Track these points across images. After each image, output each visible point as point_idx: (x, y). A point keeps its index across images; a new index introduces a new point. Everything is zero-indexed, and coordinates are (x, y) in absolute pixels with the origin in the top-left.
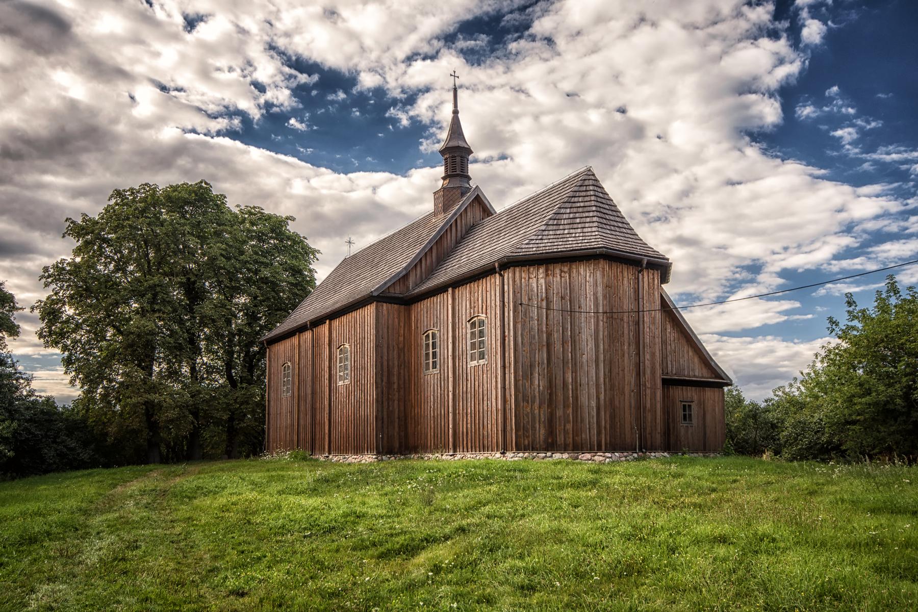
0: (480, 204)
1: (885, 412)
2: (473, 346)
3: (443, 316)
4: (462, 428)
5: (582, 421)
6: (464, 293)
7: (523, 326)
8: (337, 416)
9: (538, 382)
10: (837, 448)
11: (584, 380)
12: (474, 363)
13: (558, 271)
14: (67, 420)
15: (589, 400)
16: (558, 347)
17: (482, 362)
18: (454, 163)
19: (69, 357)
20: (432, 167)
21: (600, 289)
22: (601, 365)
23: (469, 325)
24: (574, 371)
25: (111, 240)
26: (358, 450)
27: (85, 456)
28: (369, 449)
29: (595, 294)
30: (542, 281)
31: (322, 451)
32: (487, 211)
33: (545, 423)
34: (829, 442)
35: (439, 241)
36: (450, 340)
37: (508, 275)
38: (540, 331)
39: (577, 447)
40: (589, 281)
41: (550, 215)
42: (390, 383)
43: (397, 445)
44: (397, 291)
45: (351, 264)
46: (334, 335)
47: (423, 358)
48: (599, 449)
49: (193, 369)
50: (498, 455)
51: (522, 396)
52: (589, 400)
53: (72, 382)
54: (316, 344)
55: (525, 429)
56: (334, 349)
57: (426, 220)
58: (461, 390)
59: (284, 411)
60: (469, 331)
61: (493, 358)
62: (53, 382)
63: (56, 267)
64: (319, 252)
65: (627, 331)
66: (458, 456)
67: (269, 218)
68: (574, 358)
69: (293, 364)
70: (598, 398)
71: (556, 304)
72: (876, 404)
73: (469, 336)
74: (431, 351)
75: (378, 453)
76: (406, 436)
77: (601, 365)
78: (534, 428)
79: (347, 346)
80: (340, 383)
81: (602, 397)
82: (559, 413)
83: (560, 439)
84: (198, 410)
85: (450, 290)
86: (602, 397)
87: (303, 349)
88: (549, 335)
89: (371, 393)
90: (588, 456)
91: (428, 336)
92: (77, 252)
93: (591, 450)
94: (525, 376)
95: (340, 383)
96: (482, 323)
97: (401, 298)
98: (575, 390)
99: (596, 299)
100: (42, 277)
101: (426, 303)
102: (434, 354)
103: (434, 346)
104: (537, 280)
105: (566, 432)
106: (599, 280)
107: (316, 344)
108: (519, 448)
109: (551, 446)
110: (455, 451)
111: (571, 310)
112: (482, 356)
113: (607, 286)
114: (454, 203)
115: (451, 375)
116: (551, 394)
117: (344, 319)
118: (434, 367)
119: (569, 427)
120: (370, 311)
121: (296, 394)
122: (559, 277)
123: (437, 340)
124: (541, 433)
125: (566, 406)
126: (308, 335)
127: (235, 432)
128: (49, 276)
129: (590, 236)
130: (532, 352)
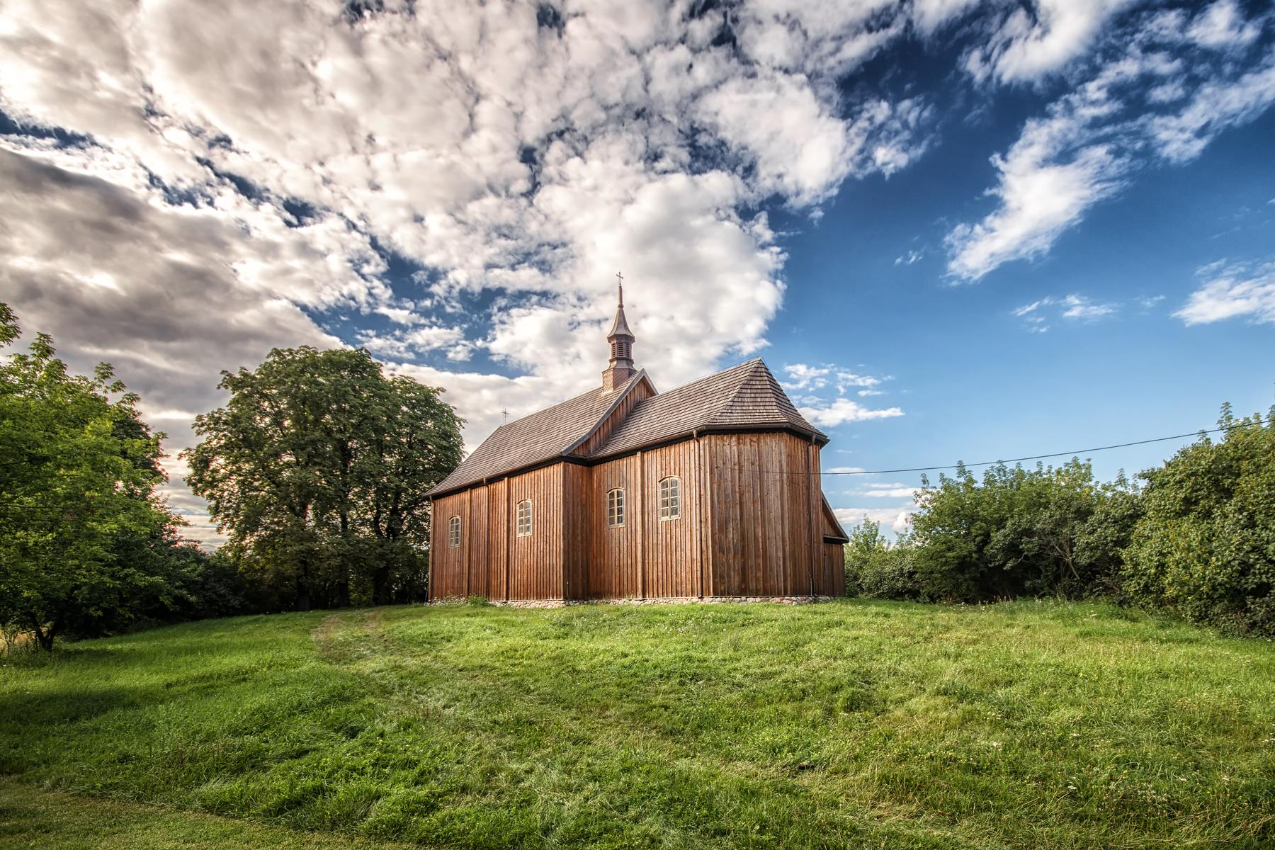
0: (646, 386)
1: (963, 564)
2: (665, 503)
3: (630, 477)
4: (651, 576)
5: (771, 569)
6: (654, 457)
7: (719, 486)
8: (516, 565)
9: (732, 535)
10: (909, 591)
11: (772, 535)
12: (666, 518)
13: (748, 441)
14: (214, 566)
15: (777, 551)
16: (749, 506)
17: (674, 517)
18: (620, 348)
19: (217, 507)
20: (483, 374)
21: (784, 457)
22: (786, 522)
23: (659, 485)
24: (763, 526)
25: (273, 396)
26: (540, 595)
27: (235, 602)
28: (555, 595)
29: (780, 461)
30: (735, 448)
31: (498, 596)
32: (650, 392)
33: (738, 568)
34: (903, 588)
35: (613, 413)
36: (639, 498)
37: (704, 441)
38: (733, 491)
39: (767, 592)
40: (775, 450)
41: (734, 393)
42: (574, 535)
43: (580, 591)
44: (581, 453)
45: (505, 434)
46: (513, 491)
47: (607, 513)
48: (786, 594)
49: (344, 522)
50: (695, 599)
51: (719, 547)
52: (777, 551)
53: (219, 530)
54: (492, 498)
55: (722, 577)
56: (513, 504)
57: (593, 395)
58: (650, 542)
59: (452, 560)
60: (660, 491)
61: (688, 514)
62: (202, 530)
63: (211, 417)
64: (465, 421)
65: (802, 491)
66: (649, 601)
67: (422, 388)
68: (763, 516)
69: (463, 517)
70: (784, 550)
71: (746, 465)
72: (958, 558)
73: (659, 494)
74: (616, 508)
75: (565, 599)
76: (588, 582)
77: (786, 522)
78: (729, 575)
79: (529, 501)
80: (520, 535)
81: (787, 549)
82: (751, 562)
83: (752, 586)
84: (354, 556)
85: (639, 454)
86: (787, 549)
87: (474, 504)
88: (741, 495)
89: (558, 544)
90: (778, 599)
91: (612, 495)
92: (235, 402)
93: (779, 594)
94: (721, 530)
95: (520, 535)
96: (674, 483)
97: (585, 460)
98: (764, 542)
99: (781, 466)
100: (195, 425)
101: (608, 466)
102: (620, 511)
103: (619, 502)
104: (730, 446)
105: (757, 579)
106: (783, 450)
107: (492, 498)
108: (716, 594)
109: (744, 591)
110: (644, 595)
111: (761, 473)
112: (674, 512)
113: (788, 456)
114: (623, 380)
115: (639, 528)
116: (743, 547)
117: (526, 477)
118: (620, 520)
119: (760, 574)
120: (557, 470)
121: (466, 544)
122: (749, 446)
123: (623, 498)
124: (735, 580)
125: (757, 557)
126: (482, 492)
127: (394, 580)
128: (203, 425)
129: (771, 414)
130: (727, 509)
